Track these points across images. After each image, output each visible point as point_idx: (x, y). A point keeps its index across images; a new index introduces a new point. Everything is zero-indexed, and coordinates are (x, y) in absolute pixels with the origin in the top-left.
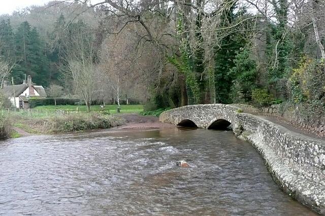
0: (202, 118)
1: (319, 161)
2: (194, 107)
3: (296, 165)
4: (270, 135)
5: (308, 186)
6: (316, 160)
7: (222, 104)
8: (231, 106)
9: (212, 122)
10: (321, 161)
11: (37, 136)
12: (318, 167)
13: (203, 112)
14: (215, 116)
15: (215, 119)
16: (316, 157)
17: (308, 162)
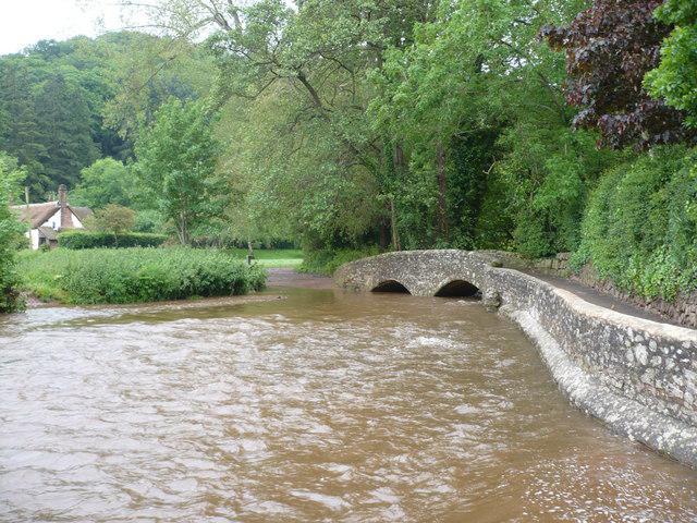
6: (630, 356)
9: (440, 285)
10: (638, 357)
12: (633, 369)
14: (448, 274)
15: (446, 281)
16: (630, 351)
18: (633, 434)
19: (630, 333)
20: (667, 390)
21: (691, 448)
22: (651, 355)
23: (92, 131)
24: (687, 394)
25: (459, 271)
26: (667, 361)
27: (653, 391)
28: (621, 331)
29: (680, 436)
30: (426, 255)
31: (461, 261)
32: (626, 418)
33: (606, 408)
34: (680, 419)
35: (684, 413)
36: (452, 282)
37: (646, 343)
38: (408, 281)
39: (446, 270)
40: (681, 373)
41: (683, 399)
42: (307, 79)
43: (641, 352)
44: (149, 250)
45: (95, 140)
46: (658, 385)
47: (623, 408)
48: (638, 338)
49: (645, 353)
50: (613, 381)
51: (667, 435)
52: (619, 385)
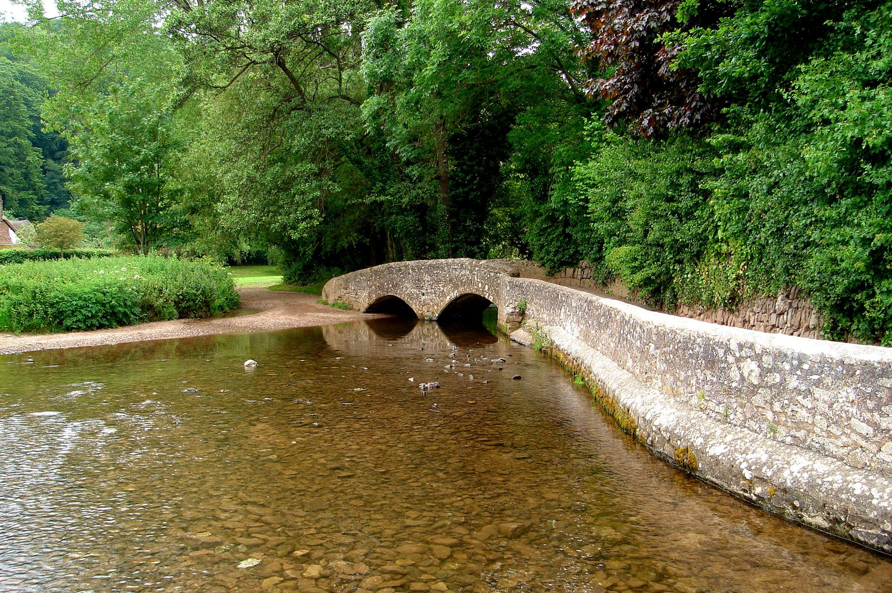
0: (424, 291)
1: (742, 375)
2: (406, 266)
3: (682, 388)
4: (599, 324)
5: (718, 434)
6: (734, 374)
7: (471, 260)
8: (177, 337)
9: (448, 300)
10: (746, 375)
11: (124, 333)
12: (740, 390)
13: (427, 278)
14: (456, 287)
15: (454, 294)
16: (734, 367)
17: (715, 379)
18: (749, 468)
19: (734, 346)
20: (789, 413)
21: (831, 483)
22: (765, 372)
23: (29, 132)
24: (818, 417)
25: (470, 282)
26: (788, 378)
27: (770, 415)
28: (720, 344)
29: (812, 470)
30: (430, 265)
31: (471, 271)
32: (736, 450)
33: (706, 438)
34: (809, 448)
35: (816, 440)
36: (462, 296)
37: (758, 358)
38: (410, 296)
39: (454, 283)
40: (808, 393)
41: (813, 424)
42: (287, 66)
43: (750, 367)
44: (83, 261)
45: (34, 145)
46: (777, 407)
47: (729, 438)
48: (745, 352)
49: (757, 371)
50: (711, 405)
51: (795, 468)
52: (721, 409)
